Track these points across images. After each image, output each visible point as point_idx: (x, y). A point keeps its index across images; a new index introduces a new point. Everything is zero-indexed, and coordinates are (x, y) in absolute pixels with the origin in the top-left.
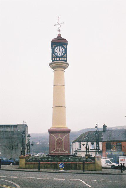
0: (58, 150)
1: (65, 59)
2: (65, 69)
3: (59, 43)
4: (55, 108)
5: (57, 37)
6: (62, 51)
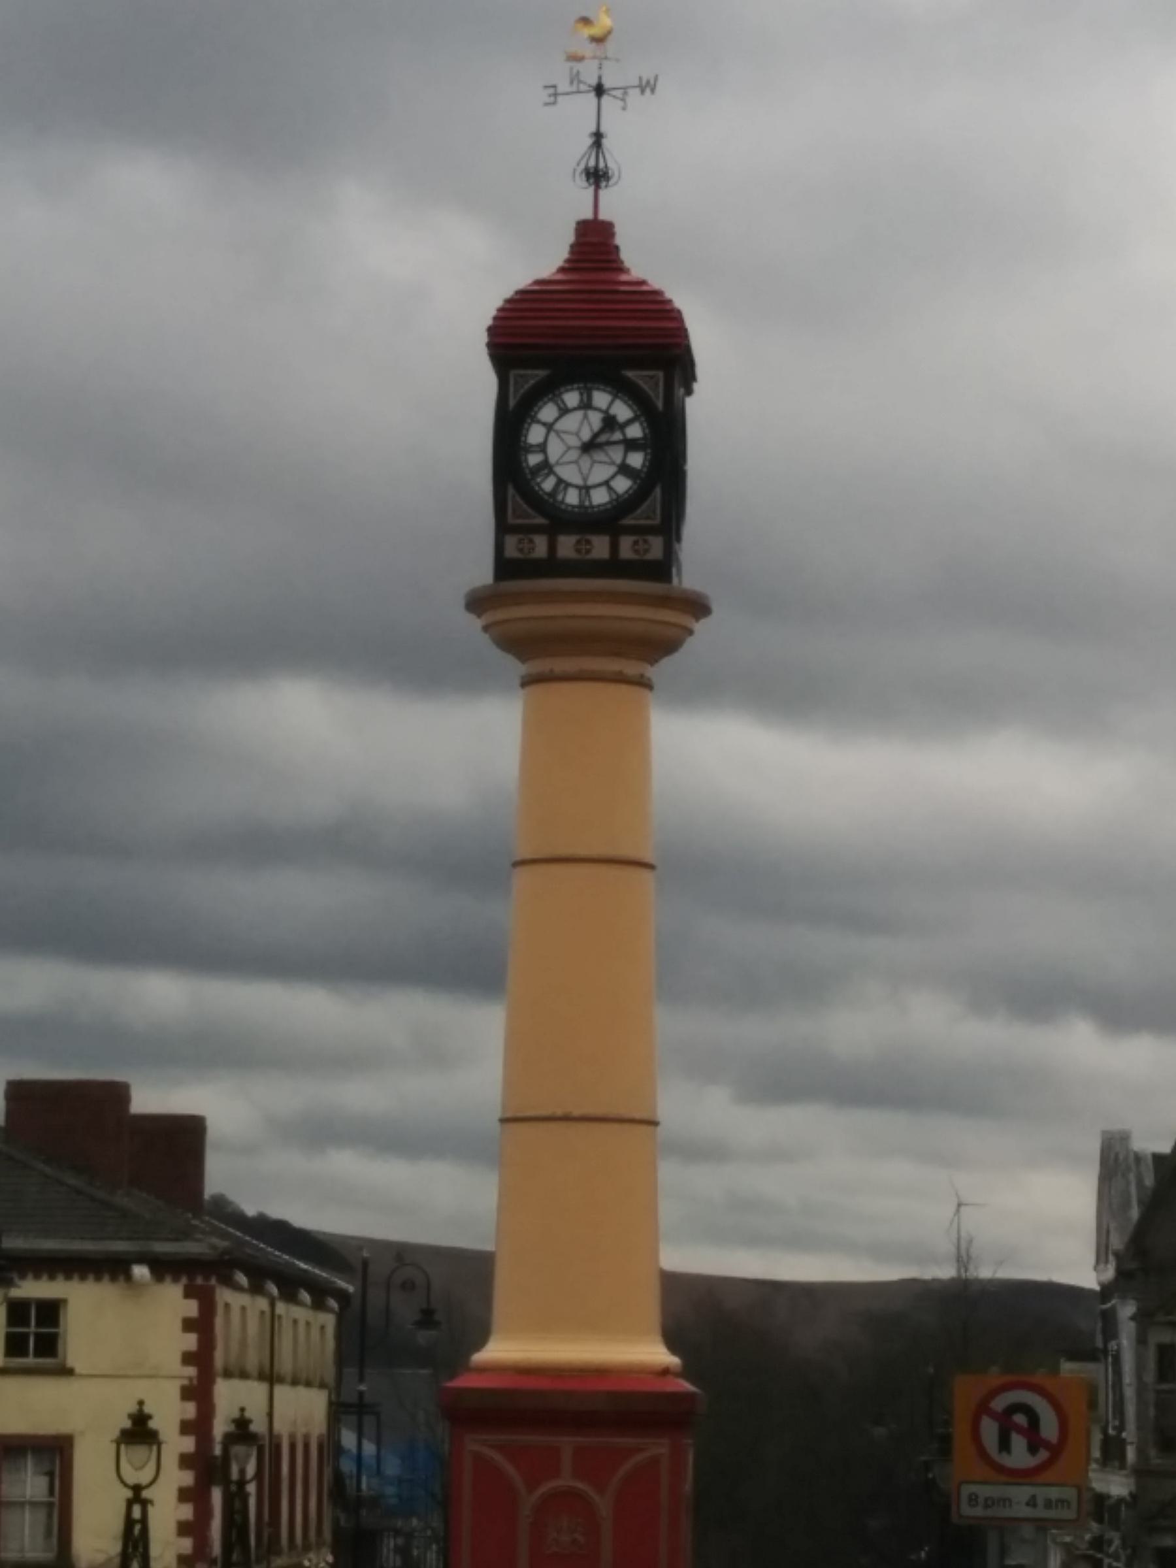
1: (511, 551)
2: (697, 619)
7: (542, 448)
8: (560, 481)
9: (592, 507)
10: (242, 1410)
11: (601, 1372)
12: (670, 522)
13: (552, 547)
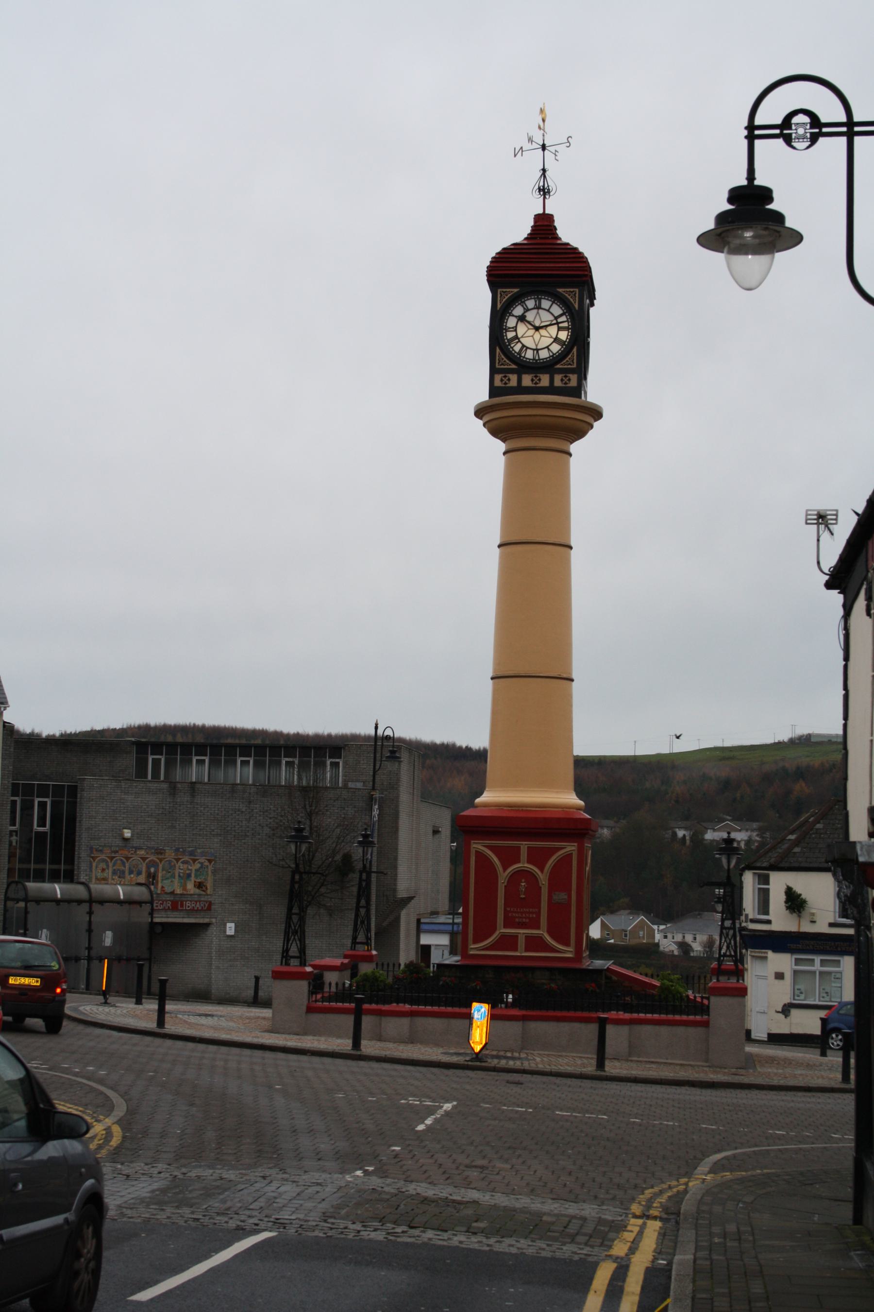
1: (498, 383)
4: (496, 680)
5: (528, 230)
7: (515, 329)
8: (523, 346)
9: (539, 359)
12: (582, 369)
13: (520, 380)
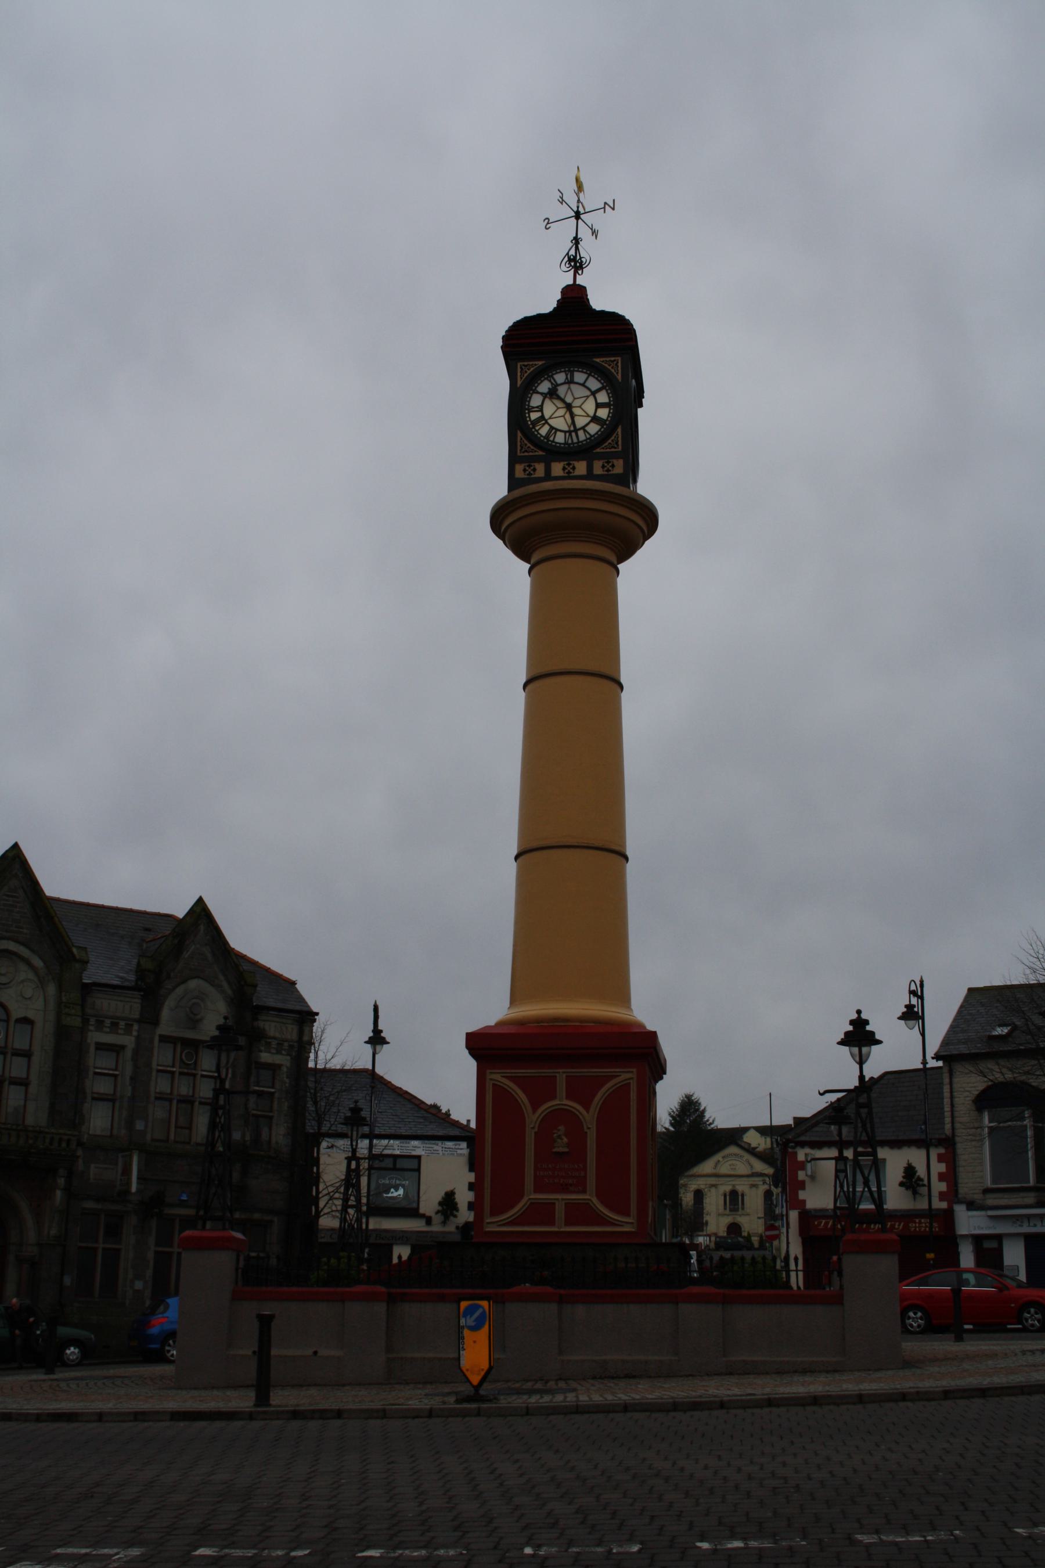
0: (568, 1223)
3: (573, 346)
6: (552, 394)
8: (552, 428)
10: (859, 1012)
11: (566, 1019)
